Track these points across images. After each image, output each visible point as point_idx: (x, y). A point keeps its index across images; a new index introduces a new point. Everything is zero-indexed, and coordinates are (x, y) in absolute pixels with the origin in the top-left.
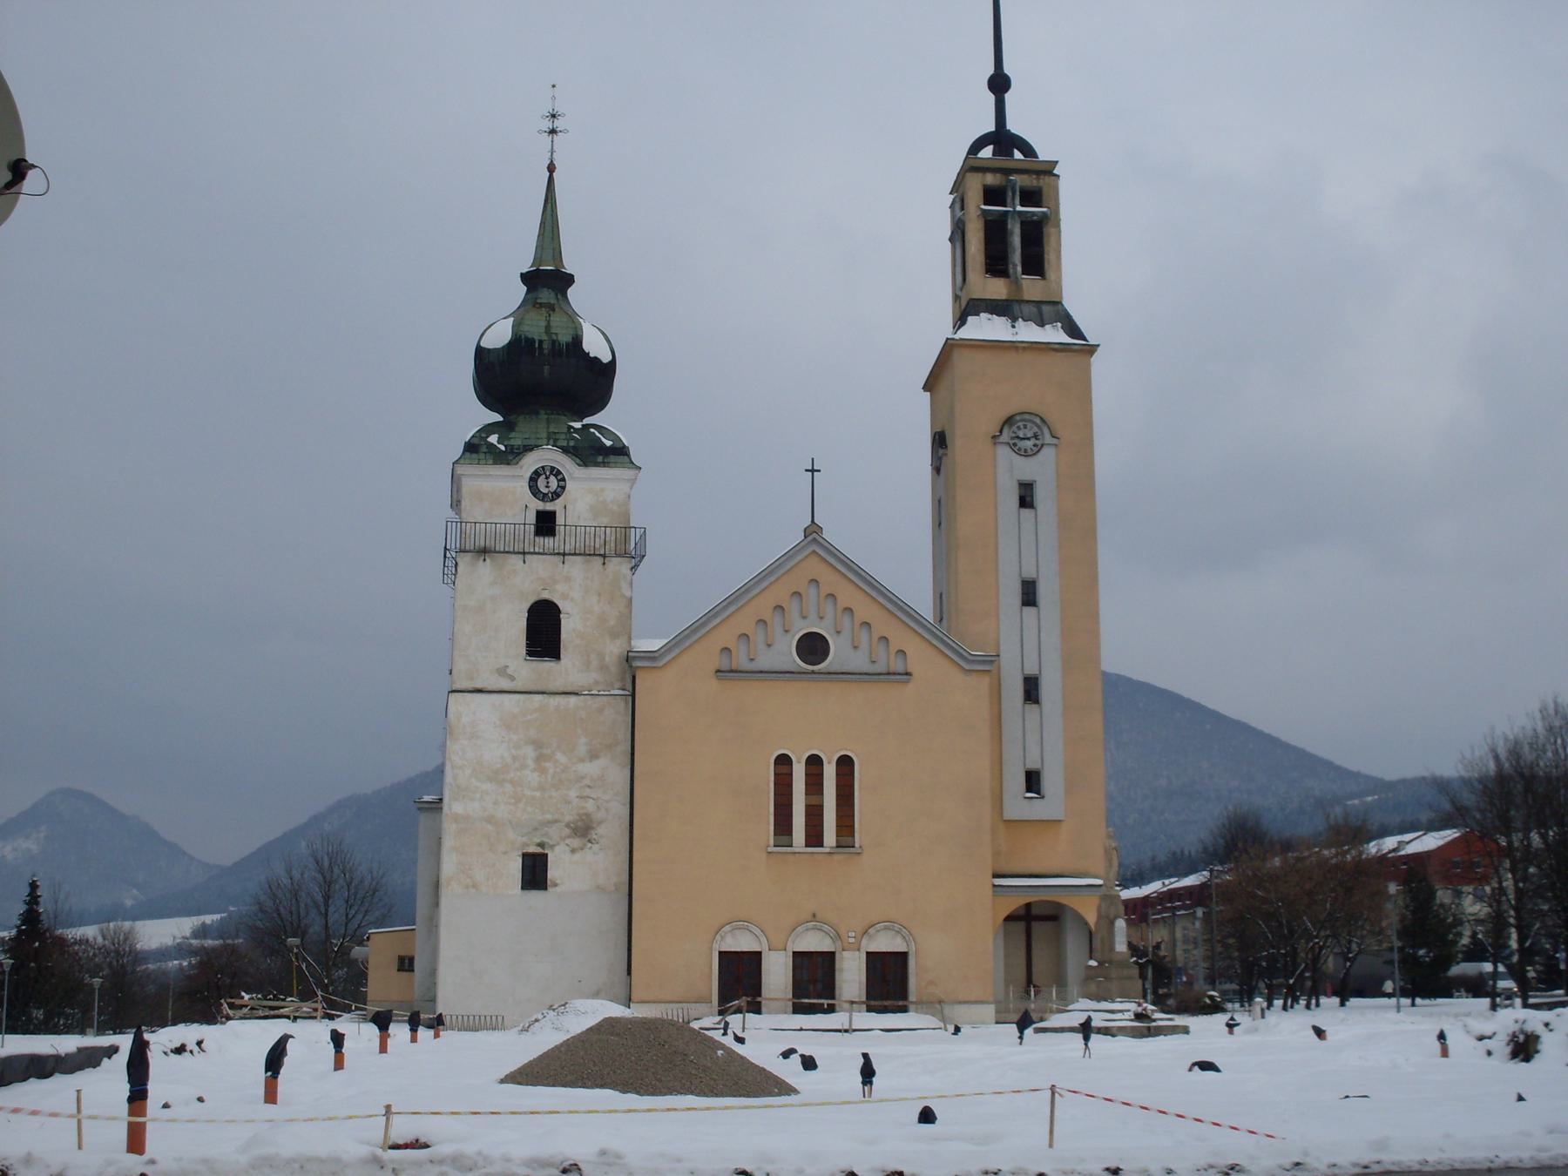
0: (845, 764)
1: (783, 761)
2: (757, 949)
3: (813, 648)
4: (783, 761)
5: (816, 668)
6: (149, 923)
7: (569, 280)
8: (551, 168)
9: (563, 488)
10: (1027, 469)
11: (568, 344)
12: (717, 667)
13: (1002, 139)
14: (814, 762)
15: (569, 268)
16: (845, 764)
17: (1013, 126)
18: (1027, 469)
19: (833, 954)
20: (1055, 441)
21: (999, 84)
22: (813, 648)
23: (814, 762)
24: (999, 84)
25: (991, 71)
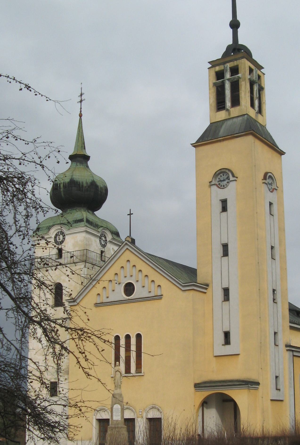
0: (139, 336)
1: (117, 338)
2: (108, 418)
3: (129, 289)
4: (117, 338)
5: (130, 297)
6: (163, 433)
7: (87, 158)
8: (81, 116)
9: (64, 239)
10: (223, 194)
11: (68, 182)
12: (95, 302)
13: (236, 50)
14: (128, 337)
15: (88, 152)
16: (139, 336)
17: (241, 42)
18: (223, 194)
19: (134, 419)
20: (234, 179)
21: (235, 25)
22: (129, 289)
23: (128, 337)
24: (235, 25)
25: (231, 19)
